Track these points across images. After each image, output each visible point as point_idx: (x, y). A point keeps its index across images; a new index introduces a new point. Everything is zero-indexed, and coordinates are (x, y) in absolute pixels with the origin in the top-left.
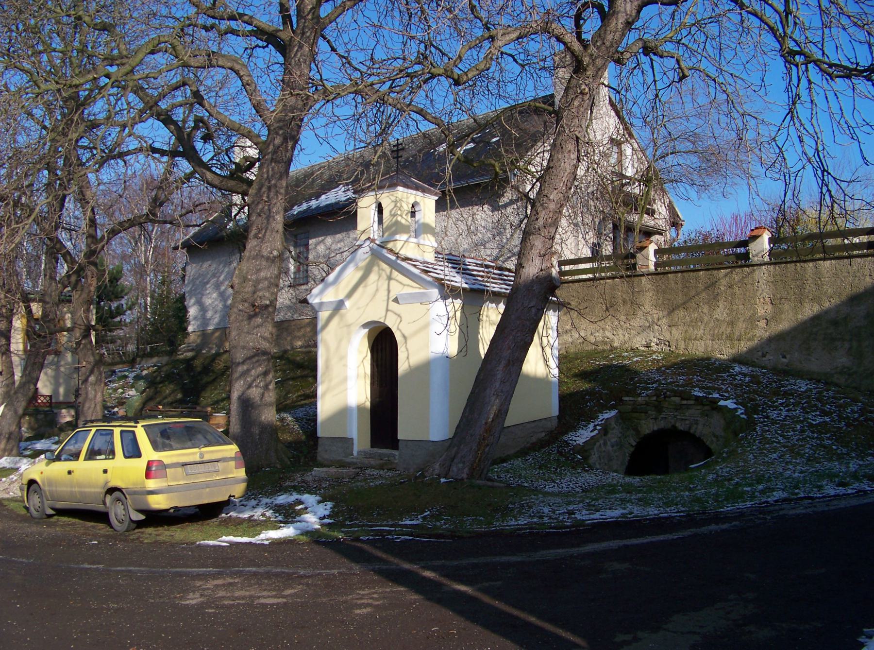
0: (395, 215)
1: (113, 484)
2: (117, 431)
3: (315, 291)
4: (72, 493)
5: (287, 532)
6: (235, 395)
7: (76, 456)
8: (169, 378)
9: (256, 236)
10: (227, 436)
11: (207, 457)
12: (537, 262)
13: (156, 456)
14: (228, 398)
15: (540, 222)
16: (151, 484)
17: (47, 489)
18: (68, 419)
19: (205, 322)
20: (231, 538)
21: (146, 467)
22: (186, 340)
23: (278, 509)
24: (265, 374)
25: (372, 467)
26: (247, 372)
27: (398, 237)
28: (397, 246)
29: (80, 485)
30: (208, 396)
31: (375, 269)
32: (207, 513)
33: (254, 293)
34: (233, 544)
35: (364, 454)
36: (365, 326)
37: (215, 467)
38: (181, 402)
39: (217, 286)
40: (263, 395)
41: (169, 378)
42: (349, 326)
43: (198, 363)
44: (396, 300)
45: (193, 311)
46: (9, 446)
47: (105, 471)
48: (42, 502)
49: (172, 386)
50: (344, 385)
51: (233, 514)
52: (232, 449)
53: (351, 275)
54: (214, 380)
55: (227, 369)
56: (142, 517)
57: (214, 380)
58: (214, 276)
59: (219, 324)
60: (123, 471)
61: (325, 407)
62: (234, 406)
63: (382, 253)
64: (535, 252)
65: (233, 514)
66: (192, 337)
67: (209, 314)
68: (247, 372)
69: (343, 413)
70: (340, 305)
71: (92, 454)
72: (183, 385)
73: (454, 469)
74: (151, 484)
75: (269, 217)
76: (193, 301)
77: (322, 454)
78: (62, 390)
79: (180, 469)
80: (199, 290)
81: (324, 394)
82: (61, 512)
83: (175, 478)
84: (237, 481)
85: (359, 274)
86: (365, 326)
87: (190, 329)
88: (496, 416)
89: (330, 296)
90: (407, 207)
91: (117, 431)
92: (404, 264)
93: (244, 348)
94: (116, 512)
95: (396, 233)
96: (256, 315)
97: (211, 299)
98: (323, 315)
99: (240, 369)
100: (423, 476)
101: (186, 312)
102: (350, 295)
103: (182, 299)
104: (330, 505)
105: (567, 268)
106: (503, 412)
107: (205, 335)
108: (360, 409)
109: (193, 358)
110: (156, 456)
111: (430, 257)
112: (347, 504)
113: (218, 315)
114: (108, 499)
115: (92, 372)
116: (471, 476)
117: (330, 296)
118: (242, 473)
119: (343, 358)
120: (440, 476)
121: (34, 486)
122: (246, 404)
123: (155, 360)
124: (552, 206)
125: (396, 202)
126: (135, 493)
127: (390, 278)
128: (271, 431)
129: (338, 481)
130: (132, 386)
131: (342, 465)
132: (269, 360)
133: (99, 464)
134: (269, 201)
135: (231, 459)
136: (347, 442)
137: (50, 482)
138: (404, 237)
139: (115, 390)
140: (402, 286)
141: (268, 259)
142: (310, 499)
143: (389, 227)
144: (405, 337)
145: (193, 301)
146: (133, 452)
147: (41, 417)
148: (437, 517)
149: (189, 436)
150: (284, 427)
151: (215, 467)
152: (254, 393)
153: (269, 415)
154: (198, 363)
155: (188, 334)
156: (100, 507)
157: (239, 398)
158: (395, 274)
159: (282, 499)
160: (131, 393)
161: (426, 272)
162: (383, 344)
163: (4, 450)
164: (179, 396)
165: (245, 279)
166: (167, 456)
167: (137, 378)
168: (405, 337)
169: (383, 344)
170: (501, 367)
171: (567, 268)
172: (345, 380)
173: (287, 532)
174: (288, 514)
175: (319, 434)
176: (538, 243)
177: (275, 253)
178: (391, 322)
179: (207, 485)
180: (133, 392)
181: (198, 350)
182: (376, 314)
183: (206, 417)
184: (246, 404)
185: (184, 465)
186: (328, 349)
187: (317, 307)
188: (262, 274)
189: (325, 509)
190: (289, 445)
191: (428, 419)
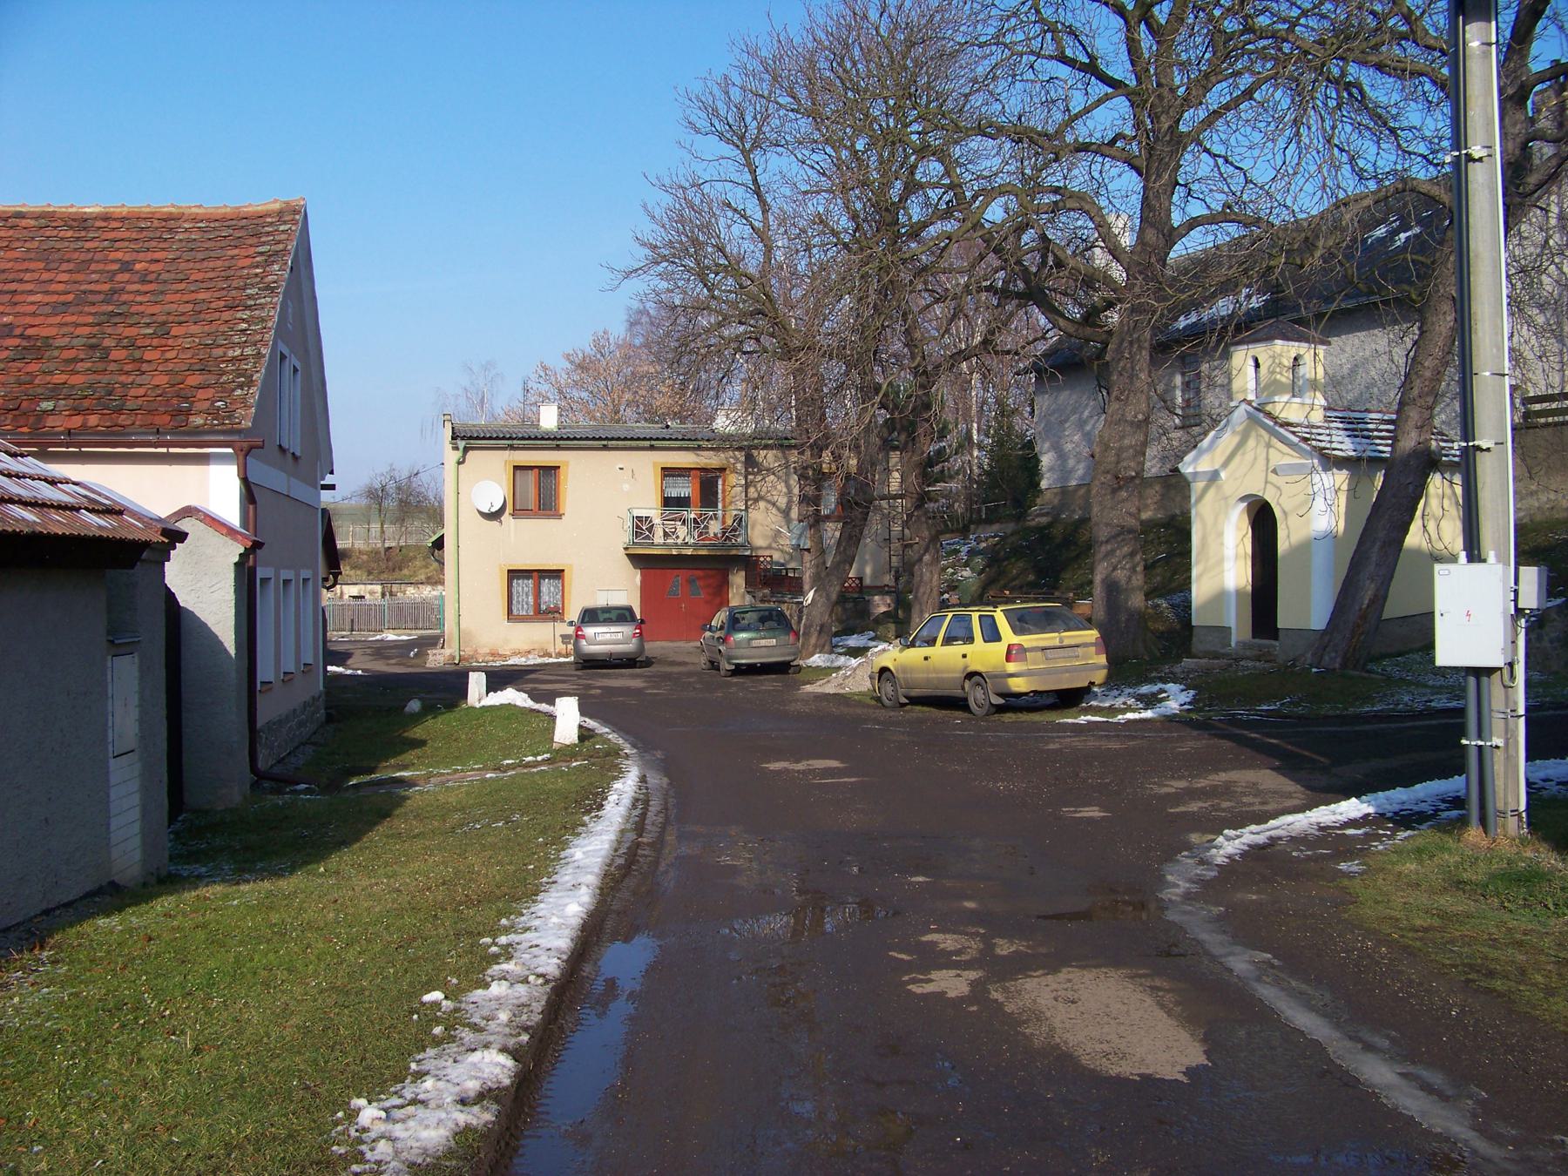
0: (1273, 372)
1: (972, 668)
2: (975, 616)
3: (1187, 458)
4: (928, 680)
5: (1148, 714)
6: (1098, 579)
7: (931, 642)
8: (1017, 552)
9: (1118, 399)
10: (1089, 622)
11: (1066, 642)
12: (1414, 434)
13: (1016, 640)
14: (1091, 582)
15: (1415, 392)
16: (1012, 667)
17: (901, 676)
18: (883, 609)
19: (1065, 473)
20: (1089, 718)
21: (1001, 650)
22: (1038, 501)
23: (1140, 698)
24: (1132, 554)
25: (1248, 658)
26: (1113, 551)
27: (1276, 399)
28: (1276, 409)
29: (936, 671)
30: (1070, 578)
31: (1253, 434)
32: (1070, 698)
33: (1118, 463)
34: (1089, 722)
35: (1244, 645)
36: (1242, 499)
37: (1076, 652)
38: (1033, 586)
39: (1081, 424)
40: (1130, 578)
41: (1017, 552)
42: (1226, 498)
43: (1057, 531)
44: (1274, 471)
45: (1046, 460)
46: (822, 641)
47: (964, 656)
48: (895, 691)
49: (1020, 564)
50: (1221, 566)
51: (1094, 703)
52: (1092, 635)
53: (1228, 440)
54: (1078, 556)
55: (1088, 548)
56: (1001, 701)
57: (1078, 556)
58: (1074, 411)
59: (1082, 478)
60: (983, 655)
61: (1200, 591)
62: (1098, 590)
63: (1262, 415)
64: (1411, 423)
65: (1094, 703)
66: (1048, 496)
67: (1071, 462)
68: (1113, 551)
69: (1220, 597)
70: (1214, 476)
71: (948, 641)
72: (1036, 558)
73: (1327, 658)
74: (1012, 667)
75: (1133, 377)
76: (1047, 445)
77: (1197, 645)
78: (868, 570)
79: (1039, 654)
80: (1054, 429)
81: (1200, 576)
82: (915, 701)
83: (1035, 662)
84: (1097, 667)
85: (1236, 439)
86: (1242, 499)
87: (1044, 484)
88: (1372, 602)
89: (1205, 465)
90: (1288, 362)
91: (975, 616)
92: (1281, 430)
93: (1107, 525)
94: (976, 696)
95: (1274, 393)
96: (1120, 488)
97: (1073, 441)
98: (1197, 487)
99: (1103, 549)
100: (1294, 665)
101: (1038, 461)
102: (1225, 464)
103: (1030, 445)
104: (1192, 692)
105: (1537, 407)
106: (1380, 599)
107: (1064, 491)
108: (1239, 593)
109: (1050, 525)
110: (1016, 640)
111: (1317, 417)
112: (1207, 690)
113: (1082, 466)
114: (967, 684)
115: (926, 550)
116: (1344, 666)
117: (1205, 465)
118: (1102, 659)
119: (1220, 534)
120: (1312, 666)
121: (886, 675)
122: (1112, 588)
123: (996, 527)
124: (1428, 374)
125: (1274, 357)
126: (996, 676)
127: (1269, 446)
128: (1140, 618)
129: (1207, 672)
130: (966, 565)
131: (1216, 656)
132: (1136, 539)
133: (958, 649)
134: (1132, 356)
135: (1091, 644)
136: (1225, 631)
137: (904, 669)
138: (1285, 398)
139: (944, 569)
140: (1283, 456)
141: (1132, 423)
142: (1172, 687)
143: (1266, 387)
144: (1285, 513)
145: (1047, 445)
146: (993, 635)
147: (850, 605)
148: (1296, 704)
149: (1046, 621)
150: (1159, 616)
151: (1076, 652)
152: (1120, 575)
153: (1137, 601)
154: (1057, 531)
155: (1041, 491)
156: (958, 693)
157: (1103, 581)
158: (1274, 441)
159: (1145, 689)
160: (965, 574)
161: (1305, 440)
162: (1262, 519)
163: (816, 646)
164: (1031, 577)
165: (1107, 448)
166: (1027, 640)
167: (972, 553)
168: (1285, 513)
169: (1262, 519)
170: (1376, 549)
171: (1537, 407)
172: (1221, 561)
173: (1148, 714)
174: (1150, 701)
175: (1194, 623)
176: (1414, 414)
177: (1140, 417)
178: (1269, 497)
179: (1067, 670)
180: (967, 573)
181: (1055, 514)
182: (1255, 487)
183: (1070, 604)
184: (1112, 588)
185: (1044, 649)
186: (1202, 520)
187: (1190, 478)
188: (1126, 442)
189: (1186, 697)
190: (1161, 636)
191: (1308, 605)
